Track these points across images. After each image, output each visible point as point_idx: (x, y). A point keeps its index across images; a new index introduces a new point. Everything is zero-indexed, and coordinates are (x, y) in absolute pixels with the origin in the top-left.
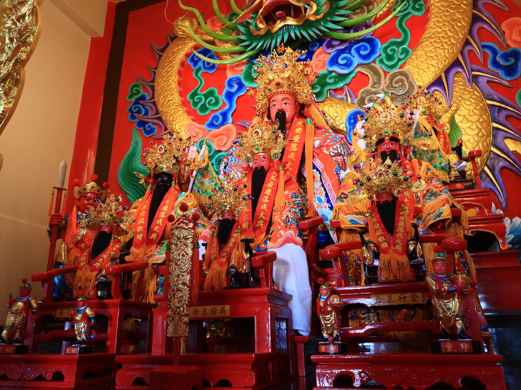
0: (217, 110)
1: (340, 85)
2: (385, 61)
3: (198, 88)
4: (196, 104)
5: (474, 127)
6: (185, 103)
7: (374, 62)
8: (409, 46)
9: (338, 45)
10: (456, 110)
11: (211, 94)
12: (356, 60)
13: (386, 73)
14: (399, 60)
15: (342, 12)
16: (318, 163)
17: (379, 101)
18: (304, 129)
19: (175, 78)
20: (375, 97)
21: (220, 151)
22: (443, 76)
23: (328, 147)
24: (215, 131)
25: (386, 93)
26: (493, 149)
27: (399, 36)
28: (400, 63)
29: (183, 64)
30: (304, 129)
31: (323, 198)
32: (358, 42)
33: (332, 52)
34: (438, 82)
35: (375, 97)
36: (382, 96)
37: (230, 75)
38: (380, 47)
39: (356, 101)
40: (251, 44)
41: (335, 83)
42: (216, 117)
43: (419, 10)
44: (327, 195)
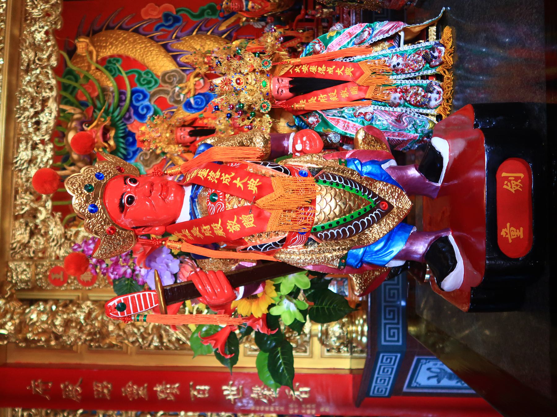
2: (150, 86)
12: (146, 102)
13: (160, 86)
14: (152, 77)
25: (175, 87)
30: (204, 118)
33: (134, 118)
34: (175, 58)
36: (177, 89)
38: (139, 87)
39: (176, 105)
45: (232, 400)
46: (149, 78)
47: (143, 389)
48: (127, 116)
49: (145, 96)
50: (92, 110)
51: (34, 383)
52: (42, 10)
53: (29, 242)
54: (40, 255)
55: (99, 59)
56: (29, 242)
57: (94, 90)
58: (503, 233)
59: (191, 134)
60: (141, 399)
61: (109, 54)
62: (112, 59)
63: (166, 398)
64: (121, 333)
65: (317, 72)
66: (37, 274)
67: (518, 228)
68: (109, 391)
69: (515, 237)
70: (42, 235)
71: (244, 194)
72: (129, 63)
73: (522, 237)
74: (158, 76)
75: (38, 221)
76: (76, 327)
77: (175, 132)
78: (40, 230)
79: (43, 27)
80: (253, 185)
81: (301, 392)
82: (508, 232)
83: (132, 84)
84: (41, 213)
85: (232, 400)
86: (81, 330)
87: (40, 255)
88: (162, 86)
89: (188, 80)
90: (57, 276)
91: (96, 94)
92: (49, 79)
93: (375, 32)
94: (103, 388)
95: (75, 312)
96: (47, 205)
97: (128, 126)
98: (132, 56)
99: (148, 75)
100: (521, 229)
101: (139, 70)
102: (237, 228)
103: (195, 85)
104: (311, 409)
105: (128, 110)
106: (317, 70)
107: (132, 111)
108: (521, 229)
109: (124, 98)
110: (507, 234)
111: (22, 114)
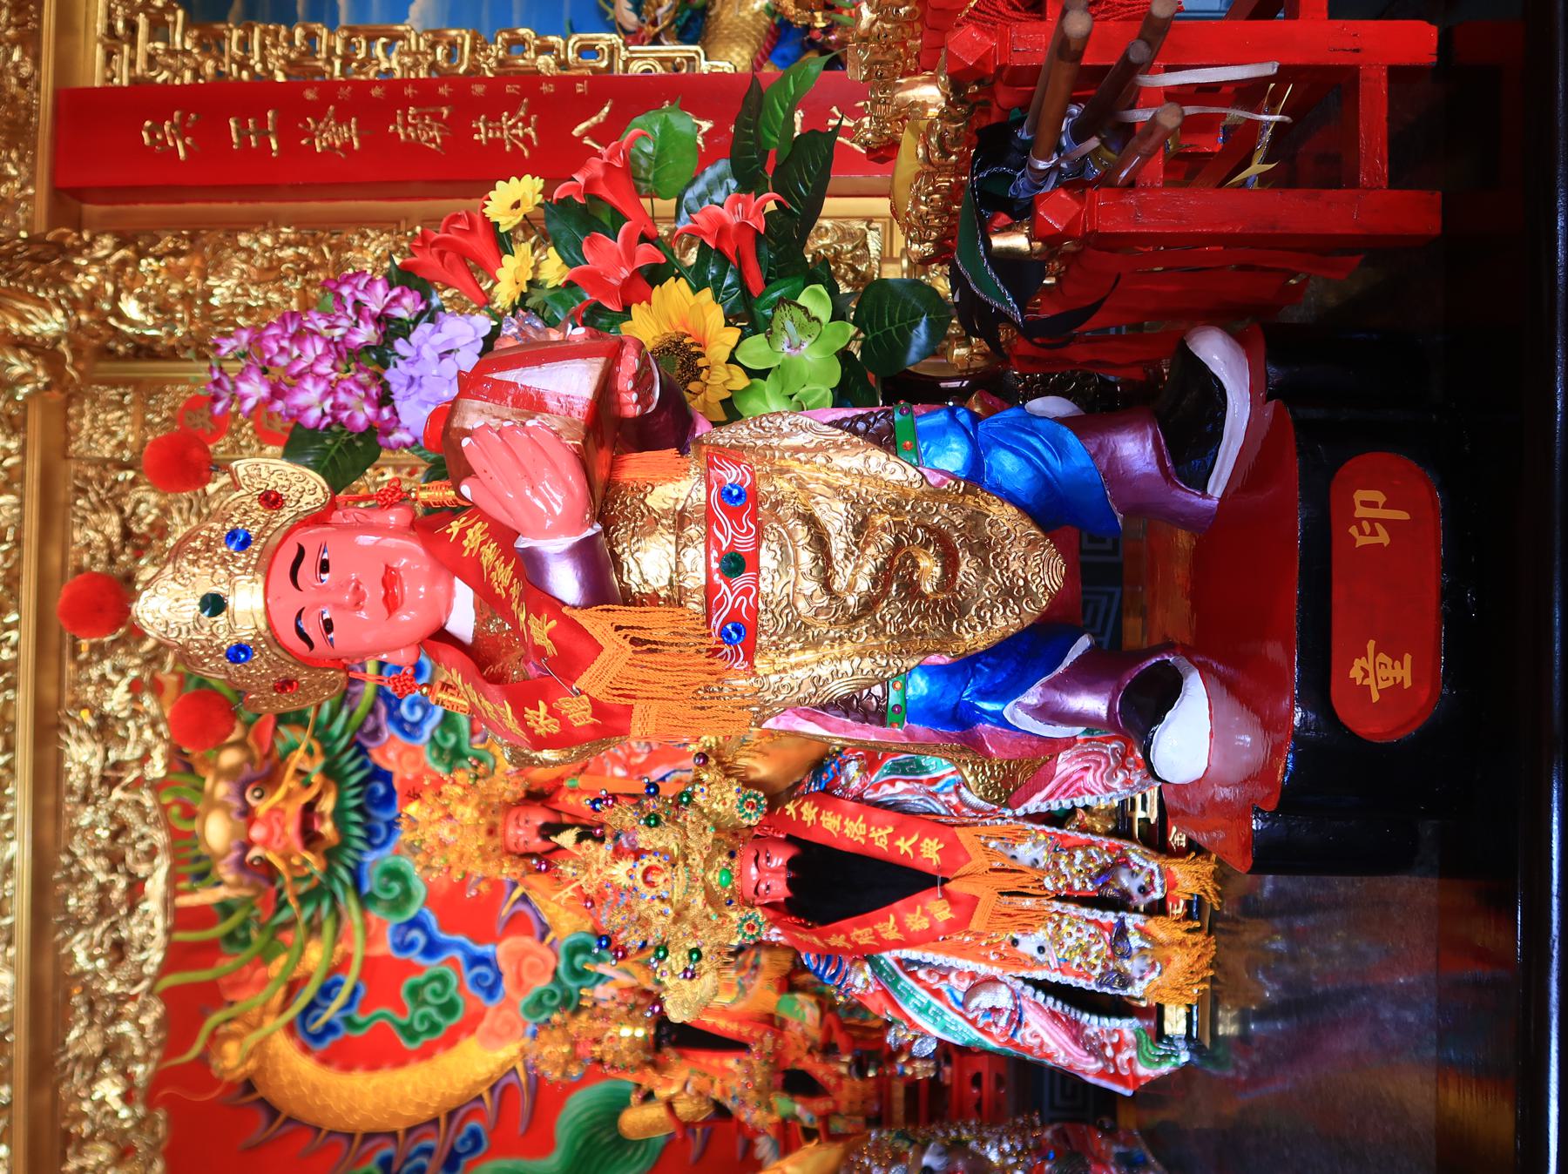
0: (460, 981)
4: (434, 1027)
6: (426, 1054)
11: (415, 991)
21: (555, 972)
24: (506, 984)
29: (324, 1060)
33: (388, 731)
37: (385, 947)
45: (77, 967)
48: (369, 727)
58: (1356, 673)
65: (841, 834)
67: (1397, 656)
69: (1391, 683)
73: (1408, 684)
77: (499, 830)
82: (1370, 668)
85: (77, 967)
100: (1408, 658)
105: (373, 710)
106: (843, 827)
107: (383, 710)
108: (1408, 658)
110: (1366, 675)
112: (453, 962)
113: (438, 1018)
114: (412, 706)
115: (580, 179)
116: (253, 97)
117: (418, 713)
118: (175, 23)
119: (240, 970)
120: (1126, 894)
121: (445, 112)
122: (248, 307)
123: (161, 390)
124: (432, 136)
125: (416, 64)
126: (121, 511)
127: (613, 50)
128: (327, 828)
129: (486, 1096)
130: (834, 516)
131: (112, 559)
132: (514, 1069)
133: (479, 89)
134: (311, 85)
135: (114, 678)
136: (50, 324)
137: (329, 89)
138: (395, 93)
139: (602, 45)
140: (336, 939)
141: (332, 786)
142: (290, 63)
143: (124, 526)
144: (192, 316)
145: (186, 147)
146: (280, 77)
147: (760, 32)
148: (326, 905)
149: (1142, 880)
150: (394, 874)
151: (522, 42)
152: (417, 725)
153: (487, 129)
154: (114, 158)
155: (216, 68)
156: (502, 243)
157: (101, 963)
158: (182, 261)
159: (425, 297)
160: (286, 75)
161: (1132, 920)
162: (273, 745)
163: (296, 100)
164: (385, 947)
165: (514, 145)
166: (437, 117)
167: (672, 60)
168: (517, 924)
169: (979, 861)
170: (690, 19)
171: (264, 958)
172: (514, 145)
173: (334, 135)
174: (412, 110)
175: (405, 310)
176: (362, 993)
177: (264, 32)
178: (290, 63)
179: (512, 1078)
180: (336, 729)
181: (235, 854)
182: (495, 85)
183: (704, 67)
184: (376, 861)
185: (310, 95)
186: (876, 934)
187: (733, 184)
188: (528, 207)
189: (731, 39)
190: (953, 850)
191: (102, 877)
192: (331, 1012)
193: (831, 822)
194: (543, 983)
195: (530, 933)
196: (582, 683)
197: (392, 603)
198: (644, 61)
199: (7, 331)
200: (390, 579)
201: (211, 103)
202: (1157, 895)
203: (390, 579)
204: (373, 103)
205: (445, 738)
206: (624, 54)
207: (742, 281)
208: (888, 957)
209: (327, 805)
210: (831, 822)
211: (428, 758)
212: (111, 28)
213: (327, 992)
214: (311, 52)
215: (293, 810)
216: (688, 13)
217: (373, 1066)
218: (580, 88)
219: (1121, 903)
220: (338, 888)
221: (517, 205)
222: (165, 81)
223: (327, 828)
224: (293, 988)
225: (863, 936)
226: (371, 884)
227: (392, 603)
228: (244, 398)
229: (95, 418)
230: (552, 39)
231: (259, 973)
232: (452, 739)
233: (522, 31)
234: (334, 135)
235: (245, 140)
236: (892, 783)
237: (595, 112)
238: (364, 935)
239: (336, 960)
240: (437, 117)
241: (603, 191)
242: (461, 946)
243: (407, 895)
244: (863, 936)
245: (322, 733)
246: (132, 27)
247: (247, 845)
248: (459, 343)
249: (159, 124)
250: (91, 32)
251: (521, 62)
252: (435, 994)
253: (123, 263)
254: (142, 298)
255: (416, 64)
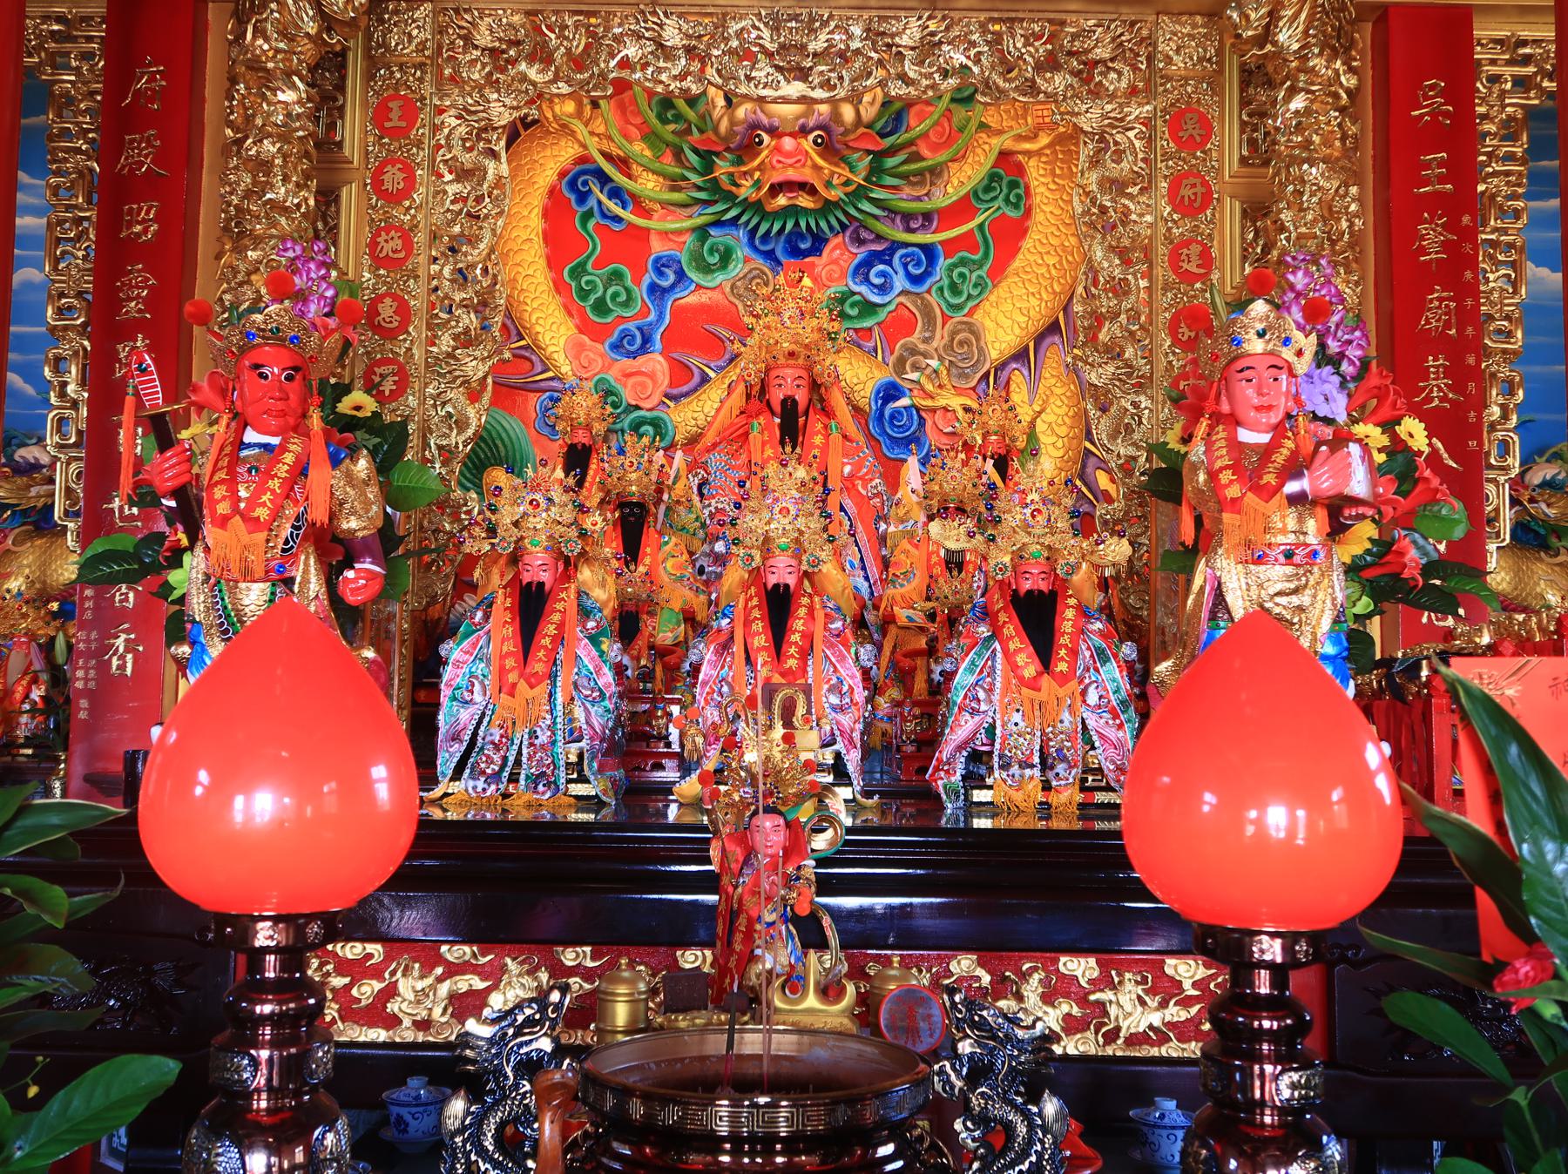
0: (628, 318)
1: (867, 324)
2: (946, 293)
3: (589, 257)
4: (584, 294)
5: (1060, 444)
6: (559, 286)
7: (929, 291)
8: (988, 273)
9: (872, 241)
10: (1040, 412)
11: (617, 276)
12: (900, 282)
13: (946, 318)
14: (970, 297)
15: (889, 181)
16: (849, 504)
17: (928, 371)
18: (827, 436)
19: (535, 222)
20: (923, 362)
21: (638, 408)
22: (1031, 345)
23: (865, 482)
24: (627, 363)
25: (941, 359)
26: (1078, 483)
27: (974, 250)
28: (970, 304)
29: (553, 192)
30: (827, 436)
31: (857, 563)
32: (907, 245)
33: (861, 253)
34: (1021, 355)
35: (923, 362)
36: (934, 363)
37: (658, 247)
38: (943, 263)
39: (892, 360)
40: (716, 202)
41: (860, 316)
42: (626, 334)
43: (1016, 206)
44: (862, 559)
46: (967, 289)
47: (140, 311)
48: (864, 234)
49: (916, 280)
50: (871, 147)
51: (158, 72)
52: (1020, 58)
53: (476, 47)
54: (447, 72)
55: (1020, 157)
56: (476, 47)
57: (936, 148)
59: (789, 405)
60: (119, 304)
61: (1033, 184)
62: (1021, 191)
63: (119, 361)
64: (240, 277)
66: (401, 67)
68: (138, 235)
70: (490, 74)
71: (253, 502)
72: (1009, 235)
74: (970, 313)
75: (523, 66)
76: (255, 182)
77: (791, 362)
78: (503, 70)
79: (977, 61)
80: (262, 513)
81: (122, 658)
83: (951, 246)
84: (540, 72)
86: (248, 194)
87: (447, 72)
88: (944, 325)
89: (959, 392)
90: (395, 115)
91: (925, 152)
92: (852, 81)
93: (588, 705)
94: (144, 224)
95: (286, 179)
96: (560, 84)
97: (839, 239)
98: (1027, 244)
99: (976, 286)
101: (986, 268)
102: (218, 496)
103: (945, 409)
104: (86, 680)
105: (879, 238)
107: (879, 247)
109: (914, 225)
111: (766, 24)
112: (645, 312)
113: (593, 298)
114: (883, 274)
115: (1427, 473)
116: (1464, 170)
117: (877, 281)
118: (1528, 98)
119: (639, 113)
120: (1052, 768)
121: (1453, 332)
122: (1302, 194)
123: (1214, 93)
124: (1432, 320)
125: (1492, 304)
126: (1112, 60)
127: (1505, 469)
128: (782, 201)
129: (522, 343)
130: (1304, 599)
131: (1070, 54)
132: (546, 370)
133: (1471, 360)
134: (1474, 220)
135: (972, 52)
136: (1288, 37)
137: (1470, 234)
138: (1469, 290)
139: (1510, 461)
140: (664, 204)
141: (819, 206)
142: (1493, 197)
143: (1103, 62)
144: (1293, 148)
145: (1422, 115)
146: (1481, 188)
147: (1525, 599)
148: (702, 195)
149: (1062, 774)
150: (726, 257)
151: (1512, 393)
152: (867, 280)
153: (1437, 367)
154: (1413, 61)
155: (1489, 133)
156: (1389, 426)
157: (735, 43)
158: (1338, 143)
159: (1354, 379)
160: (1483, 193)
161: (1037, 772)
162: (857, 150)
163: (1463, 206)
164: (658, 247)
165: (1425, 388)
166: (1448, 325)
167: (1496, 519)
168: (680, 371)
169: (1061, 692)
170: (1537, 533)
171: (649, 136)
172: (1425, 388)
173: (1432, 238)
174: (1453, 305)
175: (1345, 367)
176: (616, 227)
177: (1520, 174)
178: (1493, 197)
179: (539, 368)
180: (866, 206)
181: (765, 121)
182: (1477, 374)
183: (1492, 547)
184: (737, 241)
185: (1466, 219)
186: (1012, 638)
187: (1423, 561)
188: (1410, 442)
189: (1517, 573)
190: (1063, 679)
191: (812, 47)
192: (599, 195)
193: (1070, 613)
194: (628, 396)
195: (671, 385)
196: (1249, 494)
197: (1258, 409)
198: (1497, 496)
199: (1283, 7)
200: (1270, 408)
201: (1460, 135)
202: (1054, 783)
203: (1270, 408)
204: (1458, 270)
205: (852, 305)
206: (1502, 479)
207: (1369, 566)
208: (997, 645)
209: (805, 201)
210: (1070, 613)
211: (835, 289)
212: (1524, 43)
213: (616, 193)
214: (1502, 213)
215: (806, 175)
216: (1542, 531)
217: (547, 237)
218: (1473, 444)
219: (1045, 765)
220: (720, 207)
221: (1411, 435)
222: (1478, 91)
223: (782, 201)
224: (623, 164)
225: (1009, 630)
226: (718, 236)
227: (1258, 409)
228: (1294, 273)
229: (1192, 37)
230: (1514, 418)
231: (634, 132)
232: (854, 312)
233: (1521, 392)
234: (1432, 238)
235: (1427, 166)
236: (1089, 648)
237: (1451, 457)
238: (670, 228)
239: (648, 204)
240: (1448, 325)
241: (1420, 487)
242: (661, 317)
243: (707, 269)
244: (1009, 630)
245: (859, 193)
246: (1527, 60)
247: (773, 131)
248: (1332, 405)
249: (1442, 93)
250: (1520, 27)
251: (1494, 393)
252: (615, 295)
253: (1336, 96)
254: (1308, 111)
255: (1492, 304)
